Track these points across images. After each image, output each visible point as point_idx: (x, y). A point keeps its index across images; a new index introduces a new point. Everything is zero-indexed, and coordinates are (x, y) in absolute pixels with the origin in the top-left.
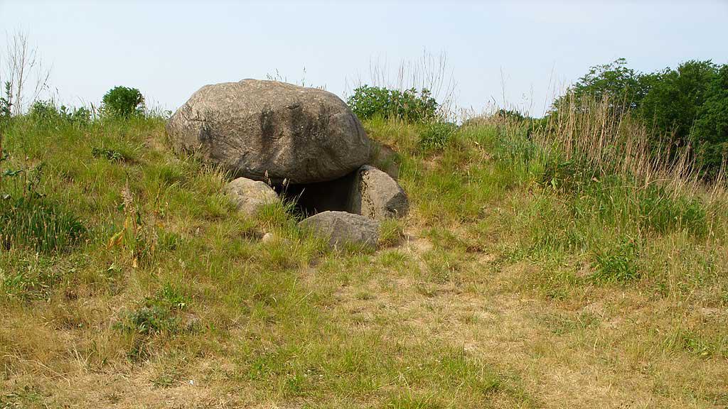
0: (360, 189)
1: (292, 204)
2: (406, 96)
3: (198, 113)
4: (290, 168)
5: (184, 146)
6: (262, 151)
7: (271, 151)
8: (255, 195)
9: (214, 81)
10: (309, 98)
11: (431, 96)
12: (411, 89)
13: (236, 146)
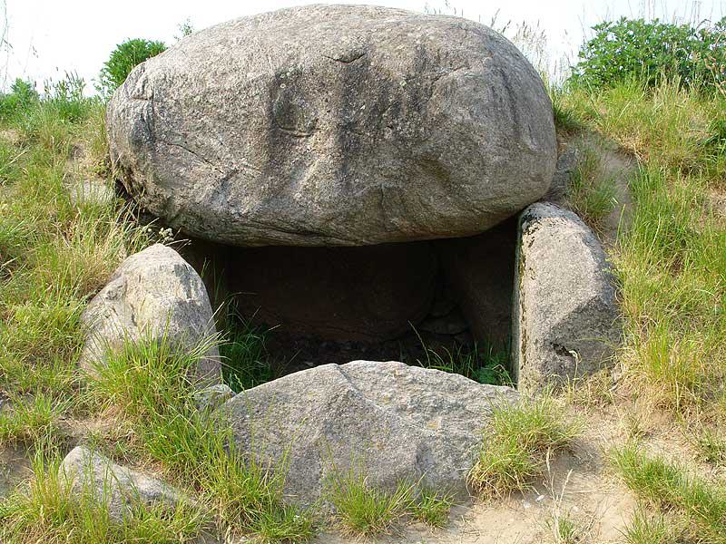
4: (330, 211)
6: (268, 170)
7: (287, 168)
13: (209, 156)
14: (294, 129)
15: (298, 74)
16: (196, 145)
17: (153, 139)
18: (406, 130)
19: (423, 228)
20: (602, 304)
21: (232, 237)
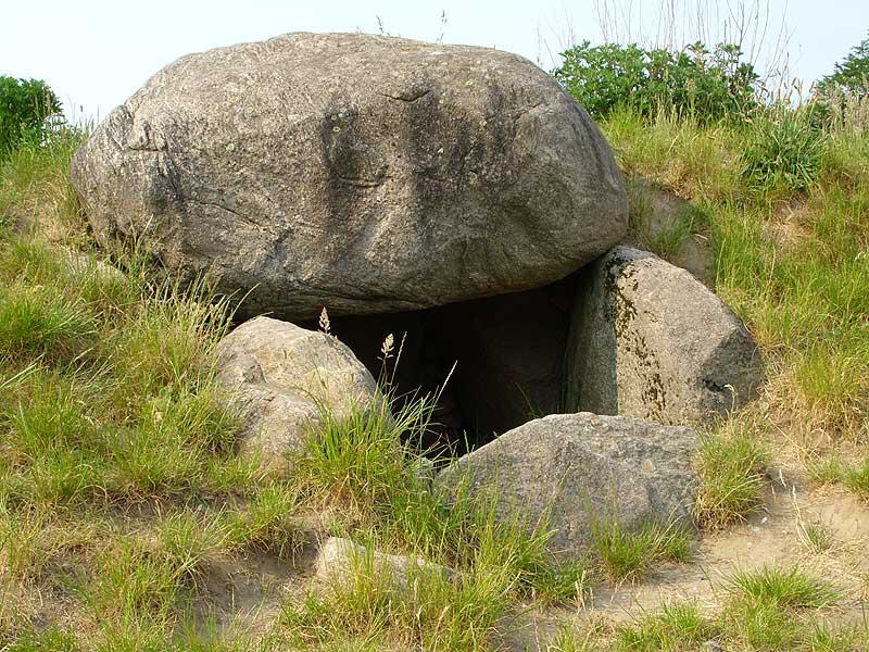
0: (610, 315)
1: (419, 410)
2: (684, 61)
3: (147, 128)
5: (113, 222)
6: (331, 226)
7: (355, 223)
8: (297, 381)
9: (200, 46)
10: (457, 68)
11: (742, 59)
12: (693, 43)
13: (254, 215)
14: (358, 179)
15: (354, 115)
16: (237, 202)
17: (181, 198)
18: (492, 174)
19: (501, 282)
20: (741, 336)
21: (282, 311)
